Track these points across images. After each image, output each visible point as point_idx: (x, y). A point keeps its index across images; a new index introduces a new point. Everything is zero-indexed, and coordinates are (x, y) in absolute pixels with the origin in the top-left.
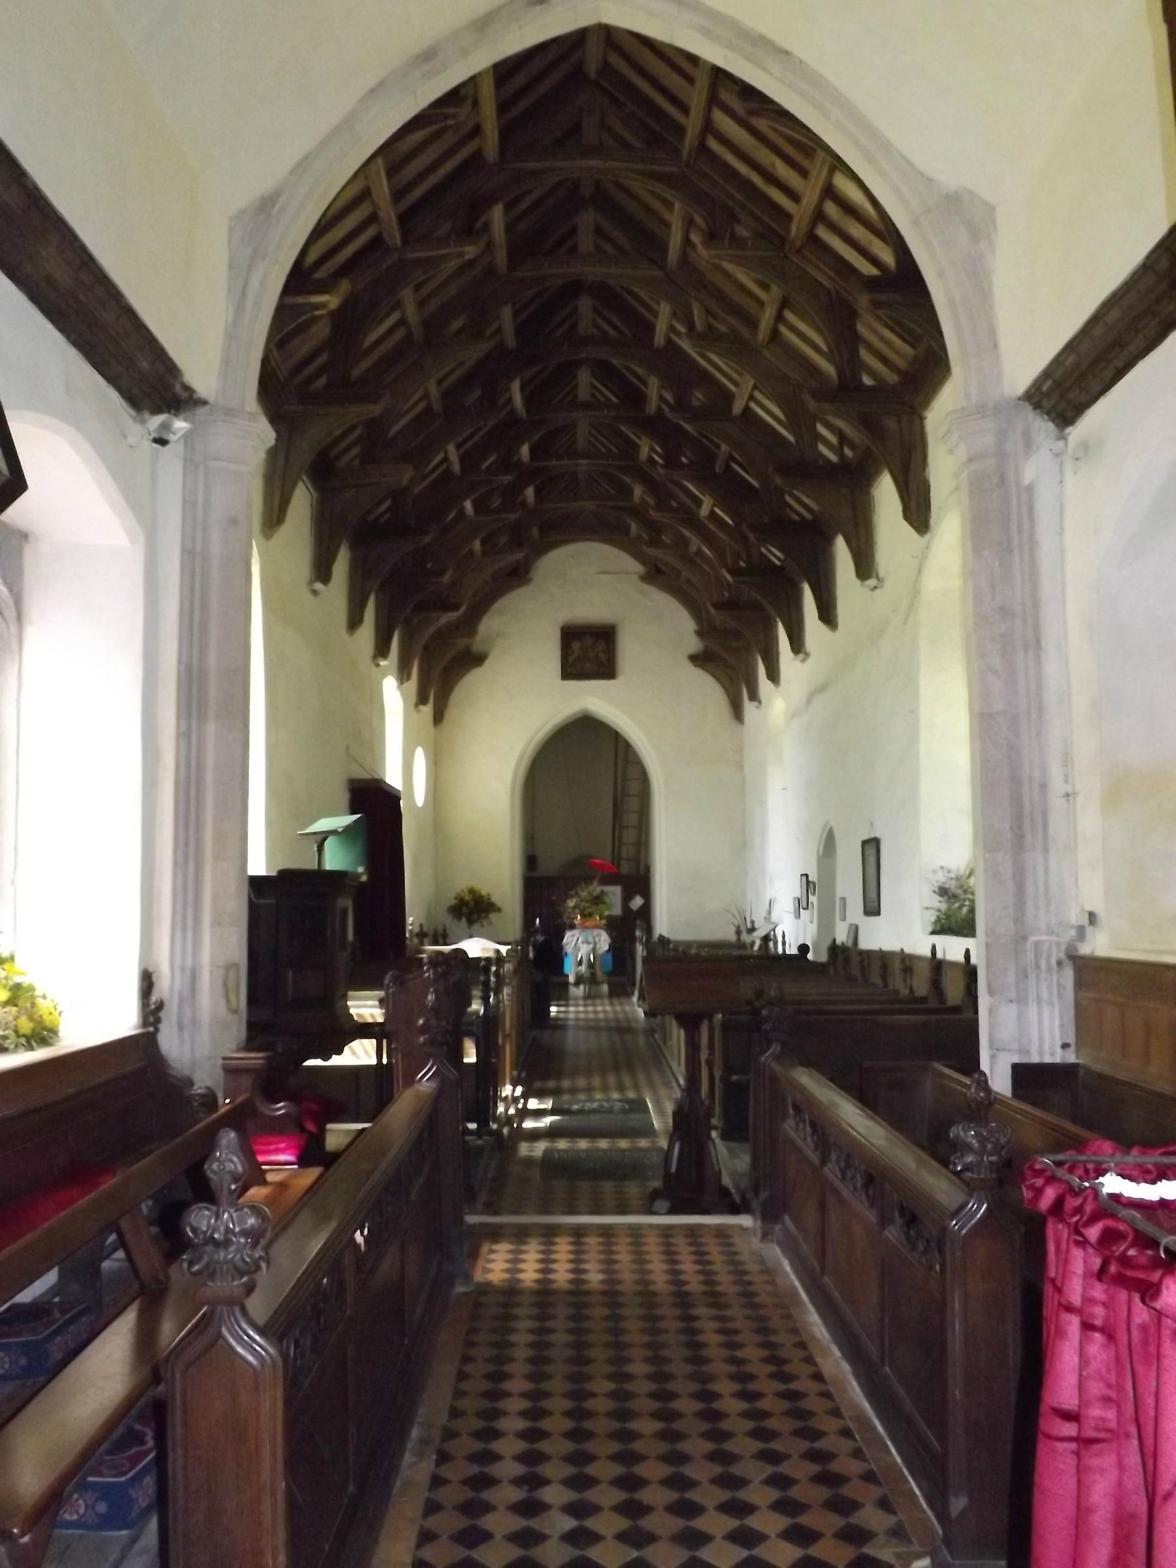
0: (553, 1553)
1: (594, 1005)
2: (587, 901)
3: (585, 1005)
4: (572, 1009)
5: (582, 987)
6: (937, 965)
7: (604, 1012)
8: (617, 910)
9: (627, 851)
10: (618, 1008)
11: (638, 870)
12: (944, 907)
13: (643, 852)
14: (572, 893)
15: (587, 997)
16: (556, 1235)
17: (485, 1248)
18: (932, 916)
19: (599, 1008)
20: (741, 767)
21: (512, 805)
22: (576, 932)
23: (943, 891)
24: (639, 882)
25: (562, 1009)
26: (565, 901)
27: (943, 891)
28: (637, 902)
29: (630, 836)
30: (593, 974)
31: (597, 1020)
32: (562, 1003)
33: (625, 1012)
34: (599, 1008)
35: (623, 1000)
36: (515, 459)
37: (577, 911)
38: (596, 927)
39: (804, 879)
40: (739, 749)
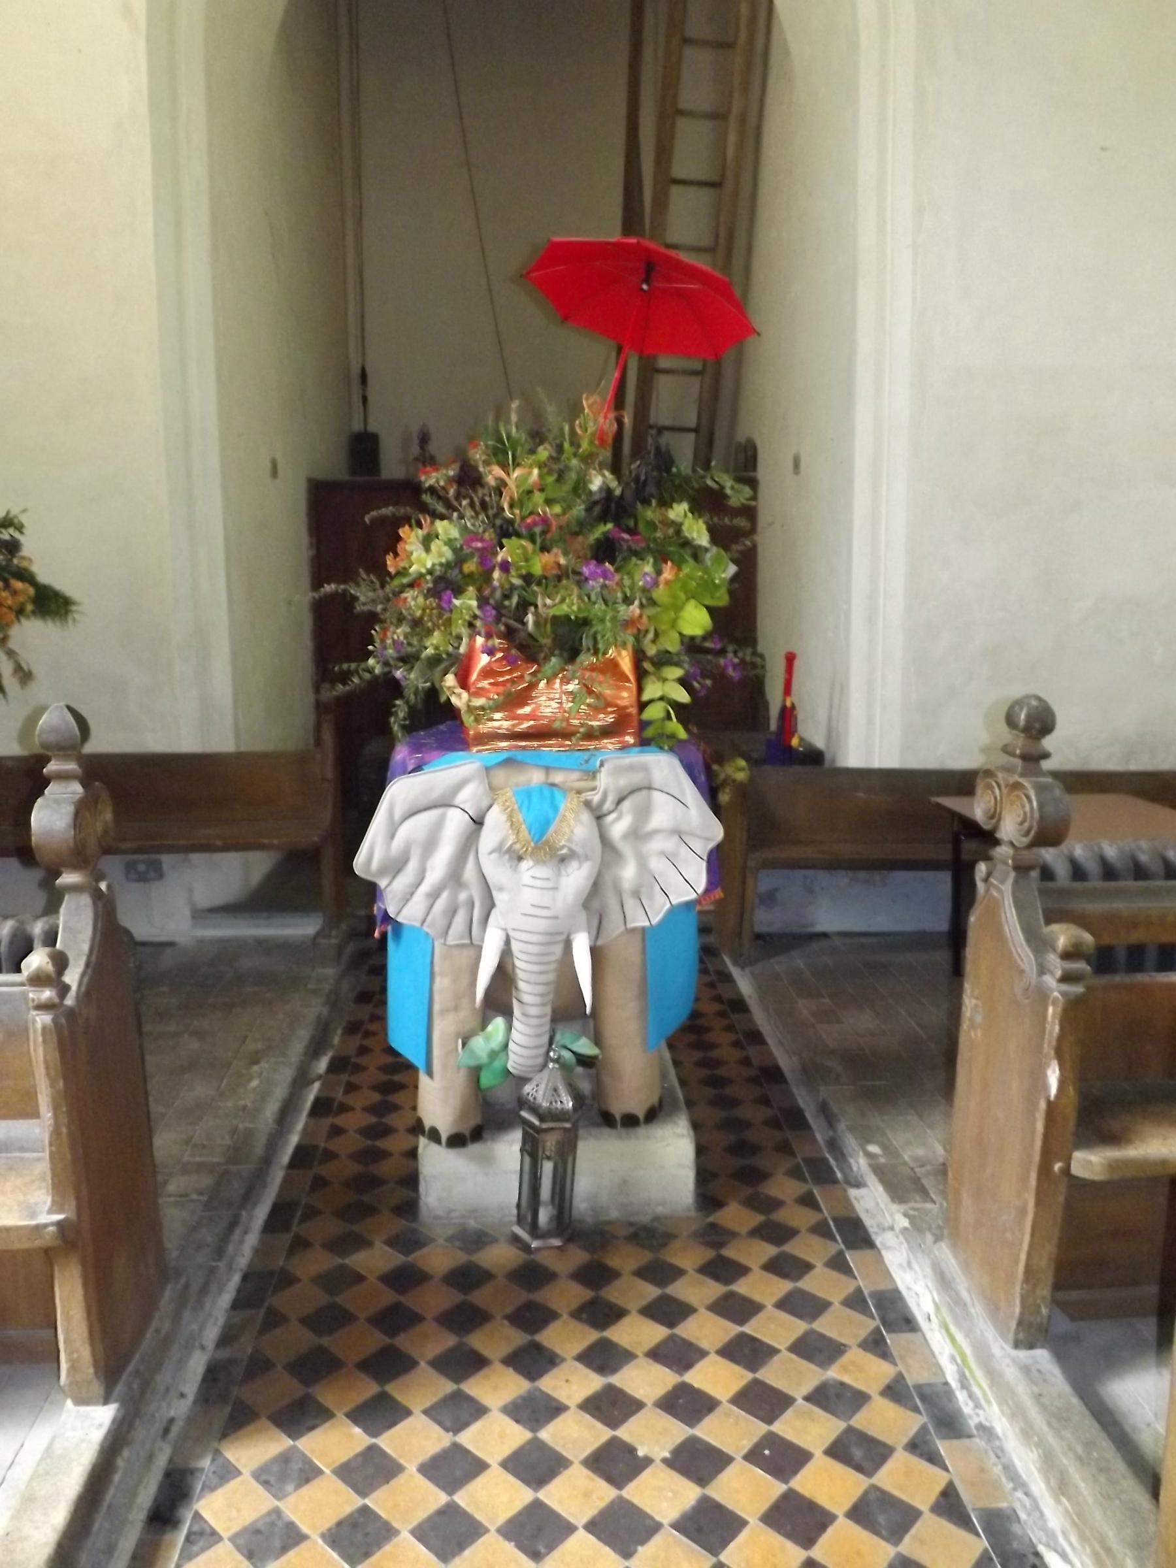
17: (1015, 1545)
22: (454, 773)
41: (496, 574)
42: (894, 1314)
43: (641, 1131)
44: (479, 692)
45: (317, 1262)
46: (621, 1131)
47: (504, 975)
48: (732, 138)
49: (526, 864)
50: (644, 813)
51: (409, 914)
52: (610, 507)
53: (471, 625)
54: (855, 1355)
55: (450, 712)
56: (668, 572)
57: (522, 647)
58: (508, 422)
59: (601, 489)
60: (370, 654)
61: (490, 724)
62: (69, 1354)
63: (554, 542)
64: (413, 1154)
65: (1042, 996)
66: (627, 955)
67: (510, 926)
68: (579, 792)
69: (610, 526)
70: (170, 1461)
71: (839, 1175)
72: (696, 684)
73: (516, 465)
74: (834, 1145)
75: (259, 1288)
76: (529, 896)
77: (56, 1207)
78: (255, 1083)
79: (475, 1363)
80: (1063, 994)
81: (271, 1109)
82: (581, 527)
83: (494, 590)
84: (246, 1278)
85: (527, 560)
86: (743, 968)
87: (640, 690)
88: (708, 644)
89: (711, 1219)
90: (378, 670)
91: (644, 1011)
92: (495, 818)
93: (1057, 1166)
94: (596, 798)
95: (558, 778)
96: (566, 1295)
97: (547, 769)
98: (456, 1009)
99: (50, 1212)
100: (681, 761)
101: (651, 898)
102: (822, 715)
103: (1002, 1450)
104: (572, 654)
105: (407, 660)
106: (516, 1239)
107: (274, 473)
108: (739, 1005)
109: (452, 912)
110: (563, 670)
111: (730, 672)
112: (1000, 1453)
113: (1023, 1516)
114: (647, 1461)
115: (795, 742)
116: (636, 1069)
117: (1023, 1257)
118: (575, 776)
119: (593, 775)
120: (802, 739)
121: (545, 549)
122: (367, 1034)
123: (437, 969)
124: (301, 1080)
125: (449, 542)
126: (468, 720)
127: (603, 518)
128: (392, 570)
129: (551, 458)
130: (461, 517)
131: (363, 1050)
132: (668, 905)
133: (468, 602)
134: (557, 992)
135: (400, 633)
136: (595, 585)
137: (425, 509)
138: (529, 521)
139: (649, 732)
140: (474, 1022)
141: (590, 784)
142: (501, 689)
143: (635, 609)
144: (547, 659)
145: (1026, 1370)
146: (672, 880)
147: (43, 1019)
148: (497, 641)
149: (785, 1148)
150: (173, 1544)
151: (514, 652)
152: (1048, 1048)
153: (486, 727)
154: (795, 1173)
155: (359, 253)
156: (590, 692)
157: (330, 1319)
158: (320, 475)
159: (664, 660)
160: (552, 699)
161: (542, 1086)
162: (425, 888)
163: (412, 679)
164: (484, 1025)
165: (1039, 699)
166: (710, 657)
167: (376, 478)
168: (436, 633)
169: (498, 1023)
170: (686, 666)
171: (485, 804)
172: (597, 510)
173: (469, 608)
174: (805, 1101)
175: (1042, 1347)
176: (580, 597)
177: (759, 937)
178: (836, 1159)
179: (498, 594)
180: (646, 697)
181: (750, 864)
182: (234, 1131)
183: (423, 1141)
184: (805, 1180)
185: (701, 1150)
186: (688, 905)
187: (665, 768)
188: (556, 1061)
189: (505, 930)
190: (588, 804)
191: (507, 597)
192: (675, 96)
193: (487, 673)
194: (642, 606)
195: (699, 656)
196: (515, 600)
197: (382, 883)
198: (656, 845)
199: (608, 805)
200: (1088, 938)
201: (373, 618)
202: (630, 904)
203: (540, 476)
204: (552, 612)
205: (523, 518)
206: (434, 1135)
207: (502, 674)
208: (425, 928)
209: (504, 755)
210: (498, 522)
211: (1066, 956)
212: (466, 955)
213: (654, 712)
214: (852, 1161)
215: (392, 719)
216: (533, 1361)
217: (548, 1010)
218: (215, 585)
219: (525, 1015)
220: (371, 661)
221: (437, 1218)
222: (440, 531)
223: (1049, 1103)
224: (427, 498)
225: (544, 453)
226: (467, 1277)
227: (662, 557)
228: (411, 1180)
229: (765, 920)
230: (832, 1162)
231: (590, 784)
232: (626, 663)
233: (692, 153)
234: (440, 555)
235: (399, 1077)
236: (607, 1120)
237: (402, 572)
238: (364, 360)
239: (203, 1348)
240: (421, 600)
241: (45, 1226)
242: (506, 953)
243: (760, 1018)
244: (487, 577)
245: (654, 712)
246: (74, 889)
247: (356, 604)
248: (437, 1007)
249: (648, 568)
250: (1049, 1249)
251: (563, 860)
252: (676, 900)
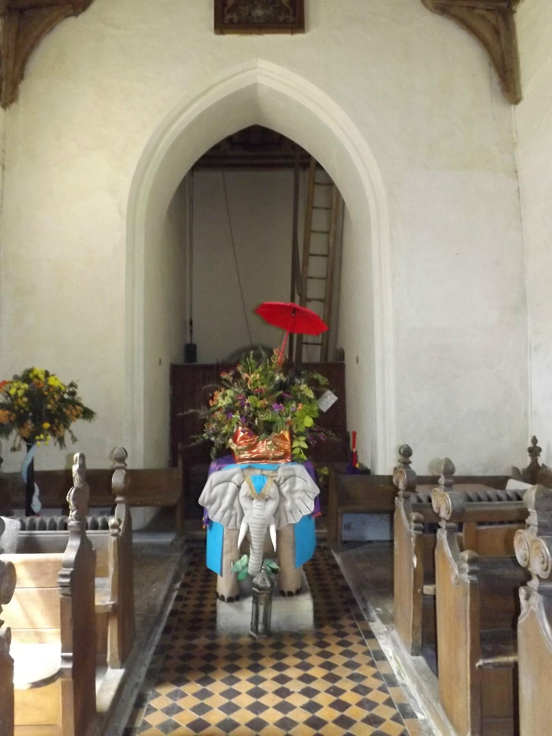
0: (390, 727)
17: (407, 711)
21: (130, 241)
22: (232, 471)
36: (328, 384)
41: (246, 407)
42: (380, 656)
43: (294, 598)
44: (240, 445)
45: (182, 642)
46: (287, 598)
47: (247, 540)
48: (332, 240)
49: (255, 501)
50: (293, 484)
51: (216, 518)
52: (282, 386)
53: (238, 423)
54: (364, 666)
55: (230, 452)
56: (300, 407)
57: (254, 430)
58: (249, 357)
59: (279, 380)
60: (204, 432)
61: (244, 455)
62: (111, 650)
63: (264, 397)
64: (215, 605)
65: (409, 535)
66: (288, 533)
67: (249, 521)
68: (272, 477)
69: (281, 392)
70: (139, 692)
71: (366, 618)
72: (311, 443)
73: (252, 372)
74: (366, 610)
75: (161, 650)
76: (256, 512)
77: (112, 599)
78: (154, 590)
79: (237, 669)
80: (415, 534)
81: (161, 598)
82: (272, 392)
83: (245, 412)
84: (157, 647)
85: (255, 402)
86: (338, 554)
87: (292, 444)
88: (315, 429)
89: (319, 631)
90: (207, 438)
91: (294, 554)
92: (245, 486)
93: (419, 590)
94: (277, 479)
95: (265, 473)
96: (267, 651)
97: (262, 470)
98: (231, 551)
99: (110, 601)
100: (306, 468)
101: (296, 512)
102: (369, 456)
103: (408, 689)
104: (269, 432)
105: (216, 434)
106: (251, 636)
107: (160, 363)
108: (336, 567)
109: (230, 517)
110: (267, 438)
111: (322, 438)
112: (407, 690)
113: (411, 704)
114: (293, 692)
115: (357, 465)
116: (293, 575)
117: (411, 622)
118: (271, 472)
119: (276, 471)
120: (360, 464)
121: (261, 399)
122: (194, 576)
123: (225, 537)
124: (170, 590)
125: (231, 397)
126: (236, 453)
127: (280, 389)
128: (211, 405)
129: (263, 370)
130: (234, 388)
131: (192, 581)
132: (301, 516)
133: (236, 416)
134: (265, 546)
135: (214, 425)
136: (277, 411)
137: (223, 386)
138: (256, 390)
139: (295, 458)
140: (237, 557)
141: (274, 474)
142: (247, 444)
143: (289, 418)
144: (261, 434)
145: (414, 661)
146: (303, 507)
147: (113, 539)
148: (246, 429)
149: (348, 611)
150: (143, 711)
151: (251, 432)
152: (413, 551)
153: (242, 456)
154: (351, 618)
155: (191, 282)
156: (275, 444)
157: (188, 657)
158: (173, 363)
159: (299, 434)
160: (263, 448)
161: (260, 578)
162: (222, 509)
163: (218, 441)
164: (240, 558)
165: (407, 445)
166: (315, 434)
167: (194, 364)
168: (226, 426)
169: (245, 557)
170: (308, 436)
171: (241, 481)
172: (278, 387)
173: (237, 418)
174: (356, 596)
175: (421, 655)
176: (272, 415)
177: (345, 542)
178: (366, 614)
179: (246, 413)
180: (293, 446)
181: (339, 511)
182: (148, 604)
183: (218, 601)
184: (354, 620)
185: (315, 604)
186: (310, 516)
187: (300, 469)
188: (265, 570)
189: (247, 524)
190: (275, 481)
191: (249, 414)
192: (310, 226)
193: (243, 438)
194: (292, 417)
195: (312, 433)
196: (251, 415)
197: (208, 507)
198: (297, 495)
199: (281, 482)
200: (421, 517)
201: (205, 421)
202: (289, 515)
203: (260, 376)
204: (263, 419)
205: (254, 389)
206: (222, 598)
207: (247, 439)
208: (221, 523)
209: (247, 465)
210: (246, 390)
211: (416, 522)
212: (234, 533)
213: (296, 451)
214: (371, 614)
215: (211, 454)
216: (256, 668)
217: (262, 552)
218: (140, 407)
219: (254, 553)
220: (205, 435)
221: (223, 630)
222: (228, 393)
223: (414, 568)
224: (223, 382)
225: (261, 369)
226: (233, 647)
227: (298, 401)
228: (214, 612)
229: (346, 535)
230: (364, 614)
231: (274, 474)
232: (287, 435)
233: (318, 244)
234: (228, 401)
235: (210, 577)
236: (282, 594)
237: (214, 406)
238: (191, 315)
239: (145, 665)
240: (221, 415)
241: (108, 605)
242: (248, 532)
243: (343, 570)
244: (242, 407)
245: (296, 451)
246: (120, 502)
247: (199, 416)
248: (224, 551)
249: (294, 405)
250: (419, 620)
251: (267, 500)
252: (304, 514)
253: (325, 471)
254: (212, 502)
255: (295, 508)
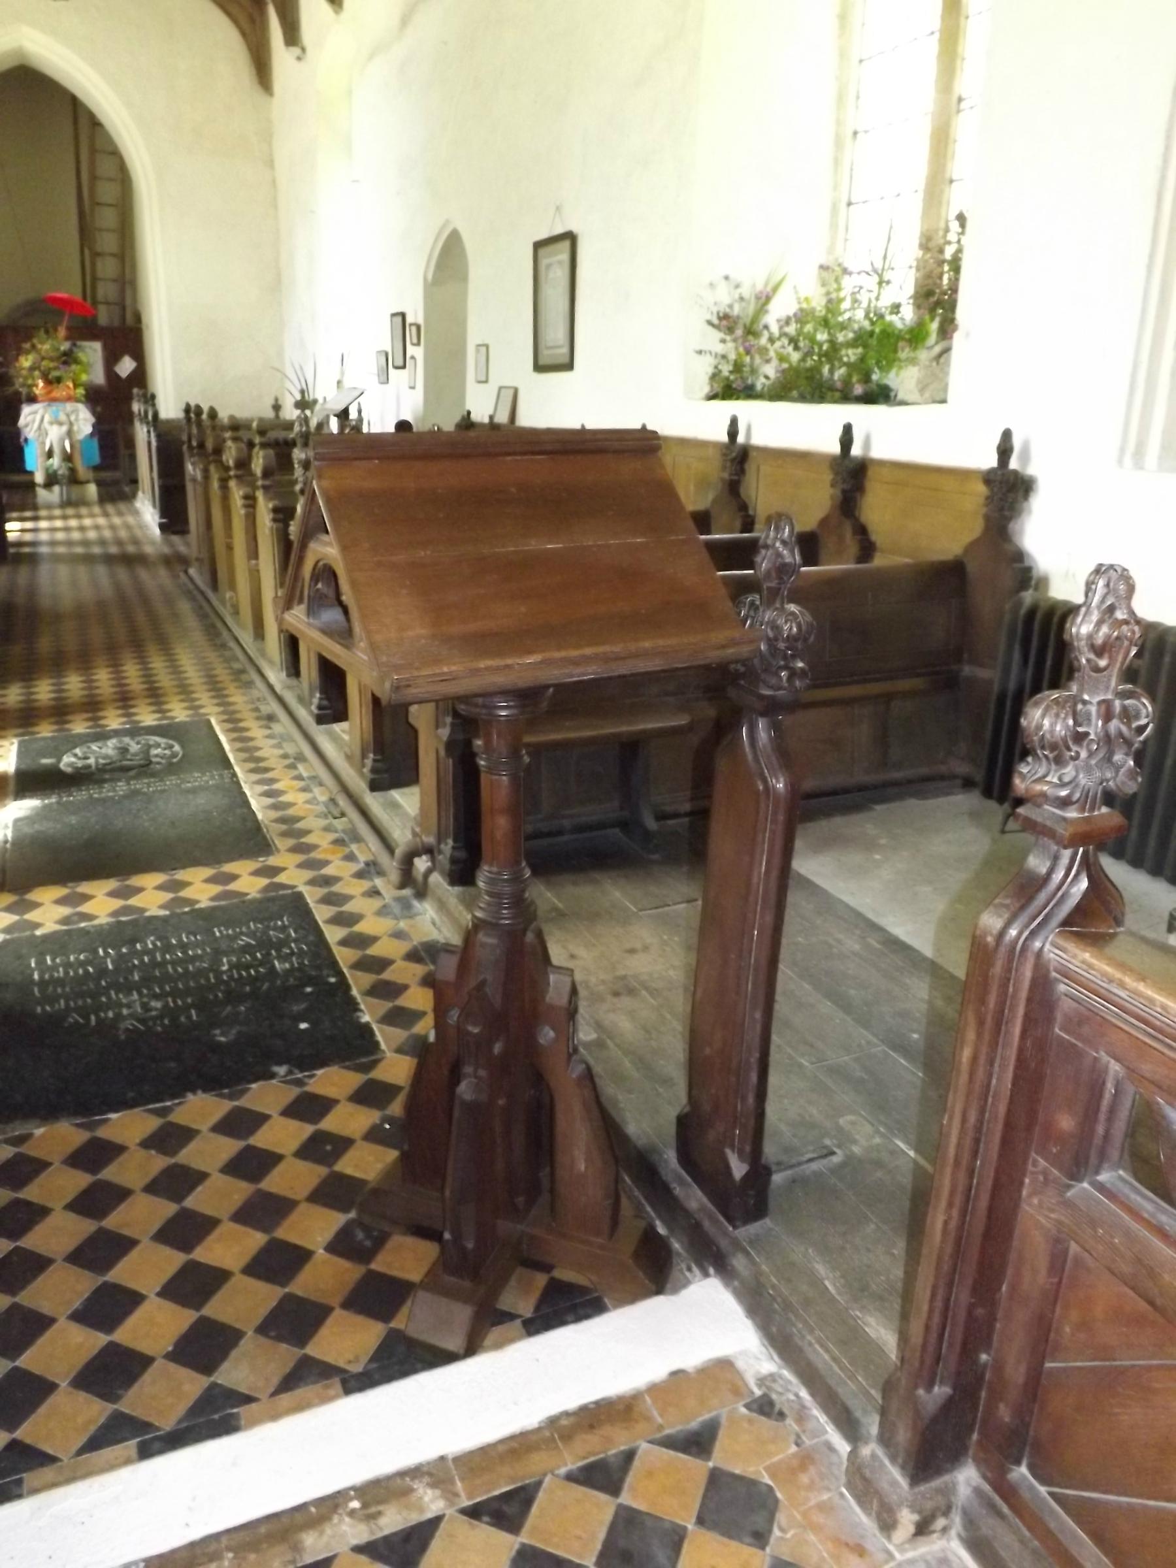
1: (79, 517)
2: (52, 359)
3: (65, 517)
4: (43, 524)
5: (56, 489)
6: (738, 457)
7: (97, 527)
8: (98, 376)
9: (106, 290)
10: (117, 521)
11: (123, 317)
12: (730, 349)
13: (128, 293)
14: (27, 346)
15: (66, 503)
16: (54, 707)
18: (703, 368)
19: (87, 522)
20: (270, 163)
23: (726, 322)
24: (127, 337)
25: (29, 525)
26: (17, 359)
27: (726, 322)
28: (126, 366)
29: (107, 268)
30: (73, 471)
31: (85, 543)
32: (28, 514)
33: (128, 527)
34: (87, 522)
35: (122, 506)
37: (37, 373)
38: (69, 399)
39: (399, 319)
40: (267, 135)
50: (77, 416)
52: (65, 354)
105: (23, 385)
232: (71, 385)
253: (99, 409)
254: (27, 426)
255: (79, 430)
